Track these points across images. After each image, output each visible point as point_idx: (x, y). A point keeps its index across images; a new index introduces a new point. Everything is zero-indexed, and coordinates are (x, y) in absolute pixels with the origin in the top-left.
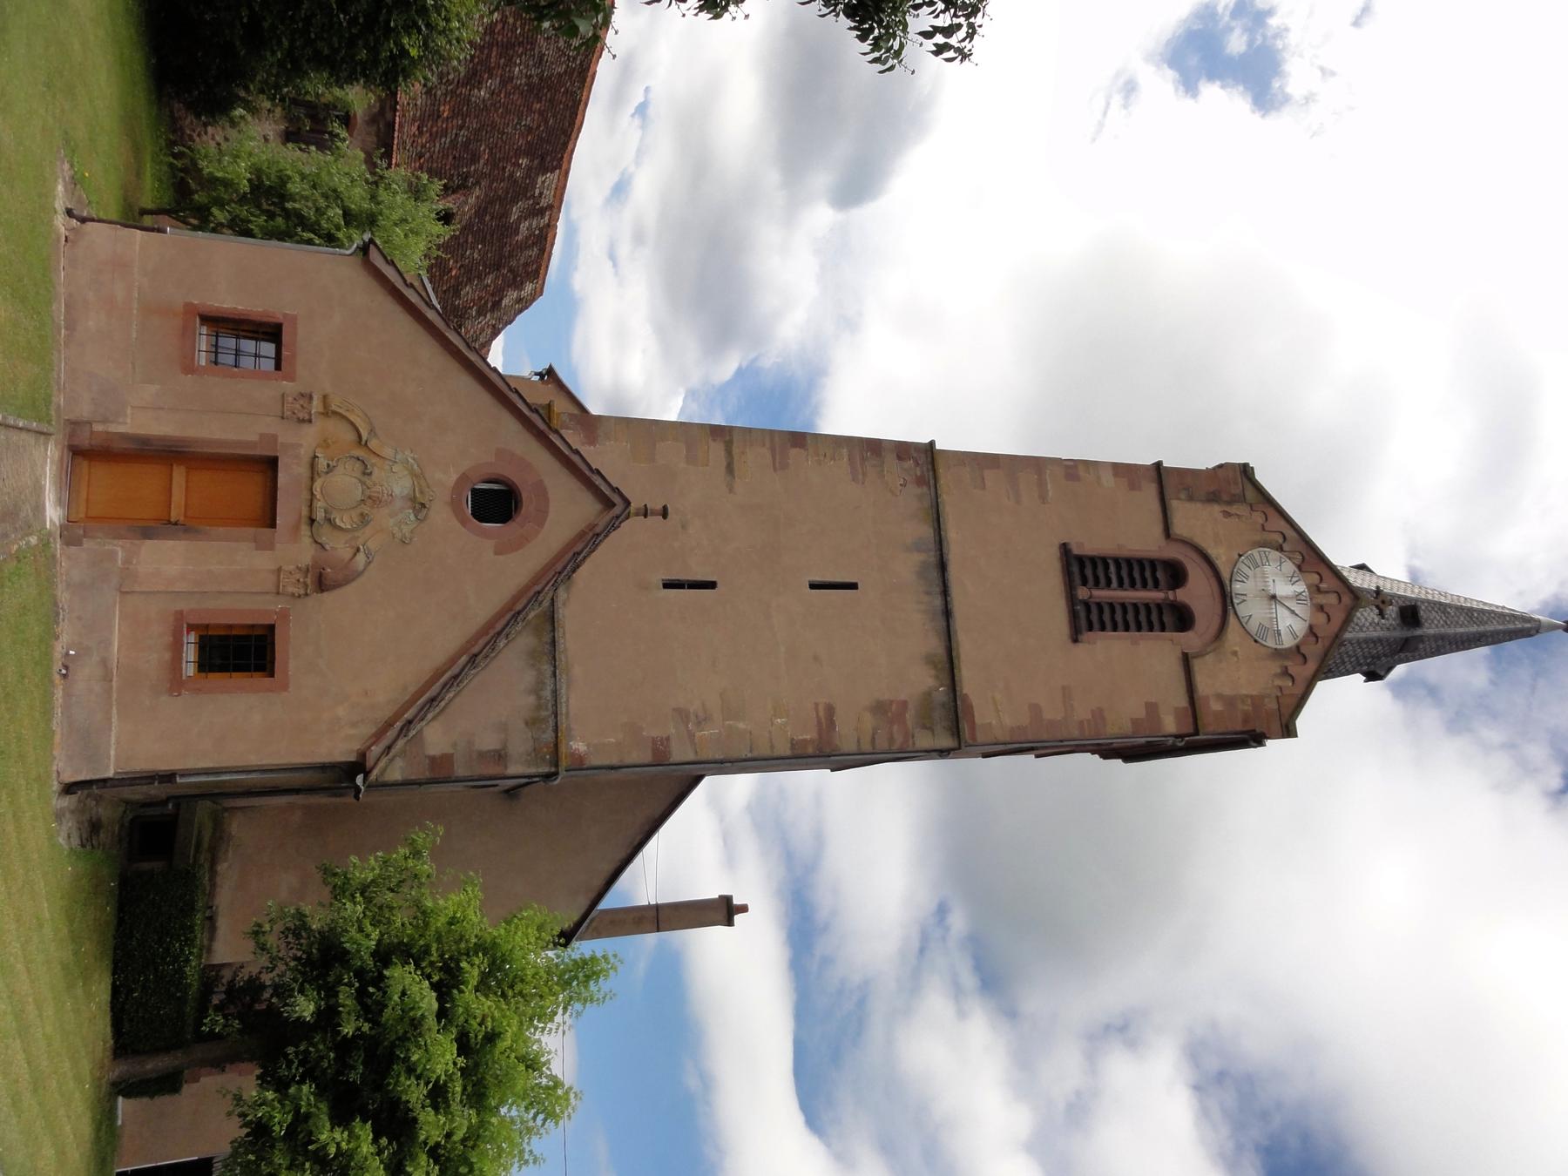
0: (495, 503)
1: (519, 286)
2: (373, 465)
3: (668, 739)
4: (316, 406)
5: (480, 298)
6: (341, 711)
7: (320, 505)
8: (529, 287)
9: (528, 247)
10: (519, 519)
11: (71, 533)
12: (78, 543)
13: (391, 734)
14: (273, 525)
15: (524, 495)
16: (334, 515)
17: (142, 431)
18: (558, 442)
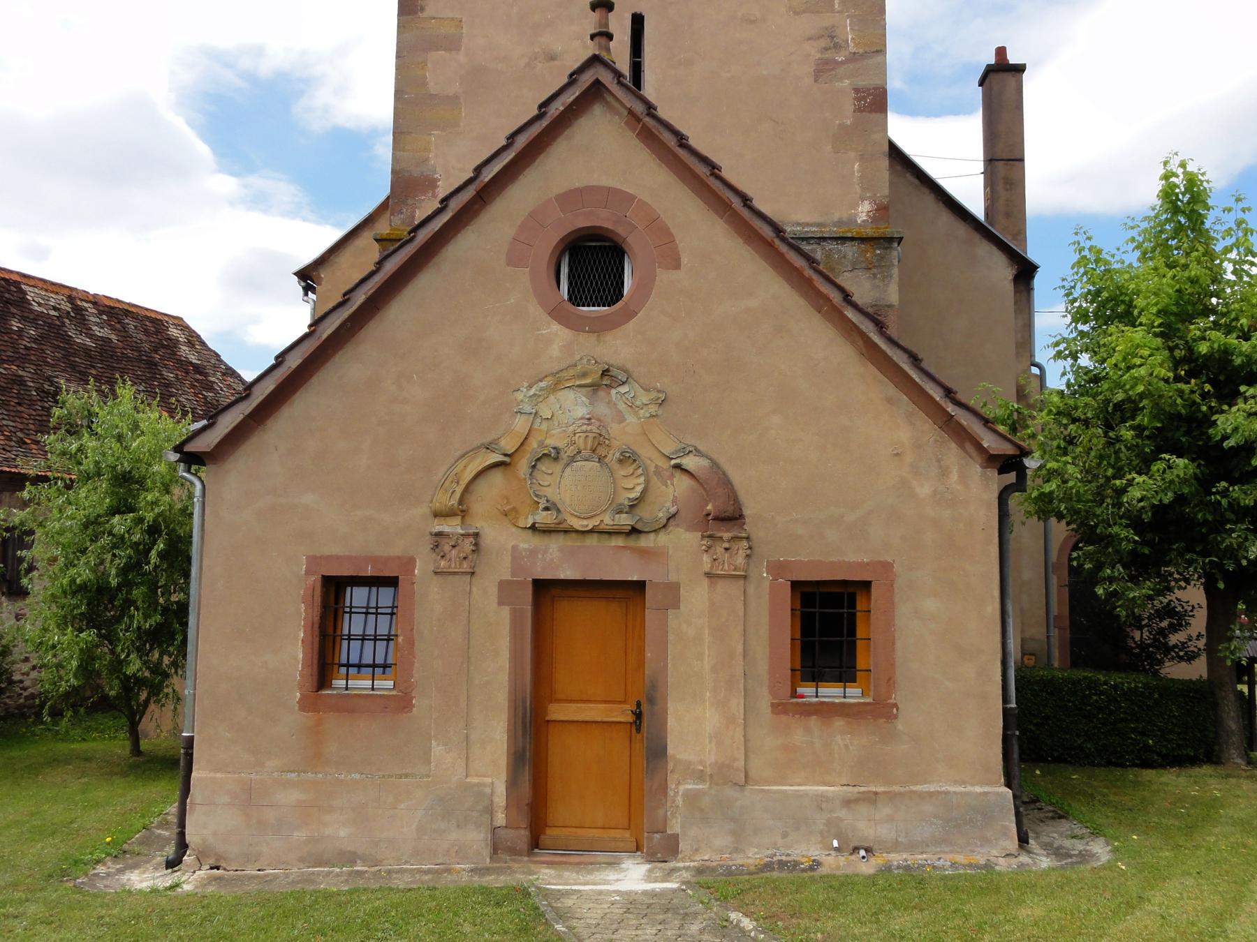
0: (593, 266)
1: (173, 344)
3: (857, 90)
4: (452, 526)
5: (193, 386)
6: (924, 490)
7: (608, 520)
8: (174, 332)
9: (124, 328)
11: (661, 850)
12: (675, 839)
13: (965, 419)
14: (640, 586)
15: (582, 223)
16: (625, 498)
17: (503, 761)
18: (496, 167)
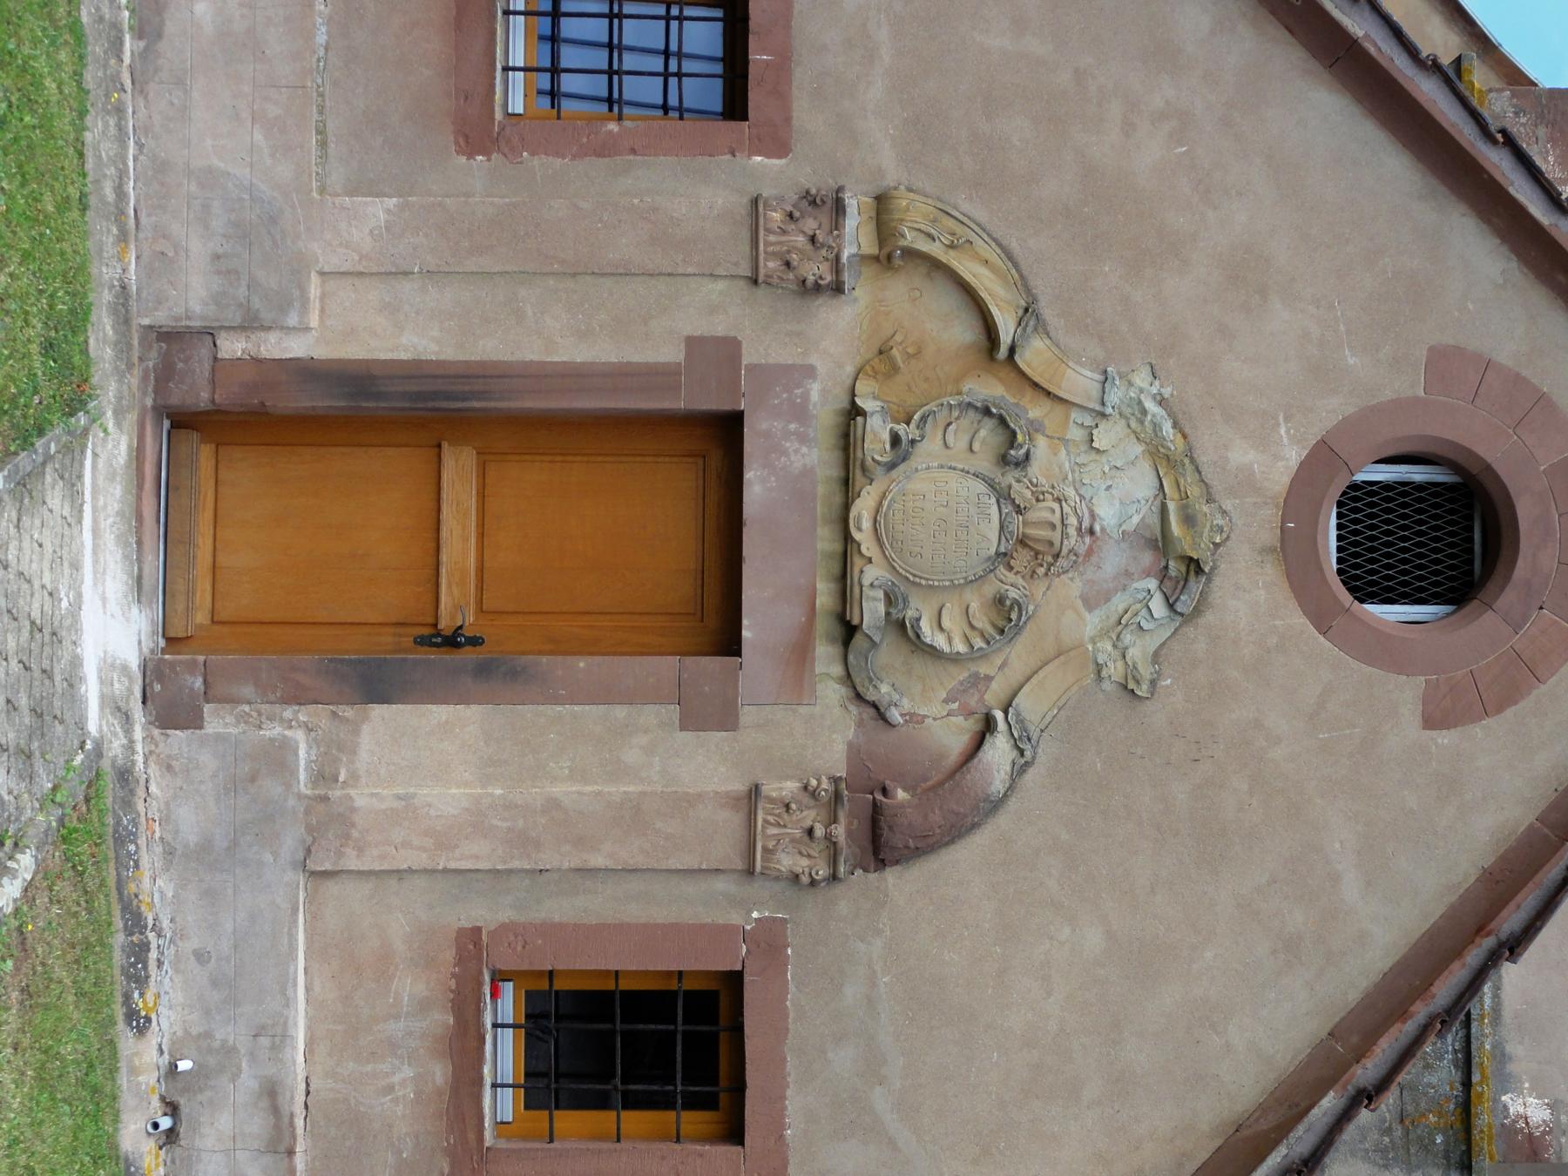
2: (1035, 427)
4: (856, 235)
7: (872, 574)
10: (1509, 598)
11: (168, 697)
12: (194, 721)
15: (1526, 511)
16: (920, 610)
